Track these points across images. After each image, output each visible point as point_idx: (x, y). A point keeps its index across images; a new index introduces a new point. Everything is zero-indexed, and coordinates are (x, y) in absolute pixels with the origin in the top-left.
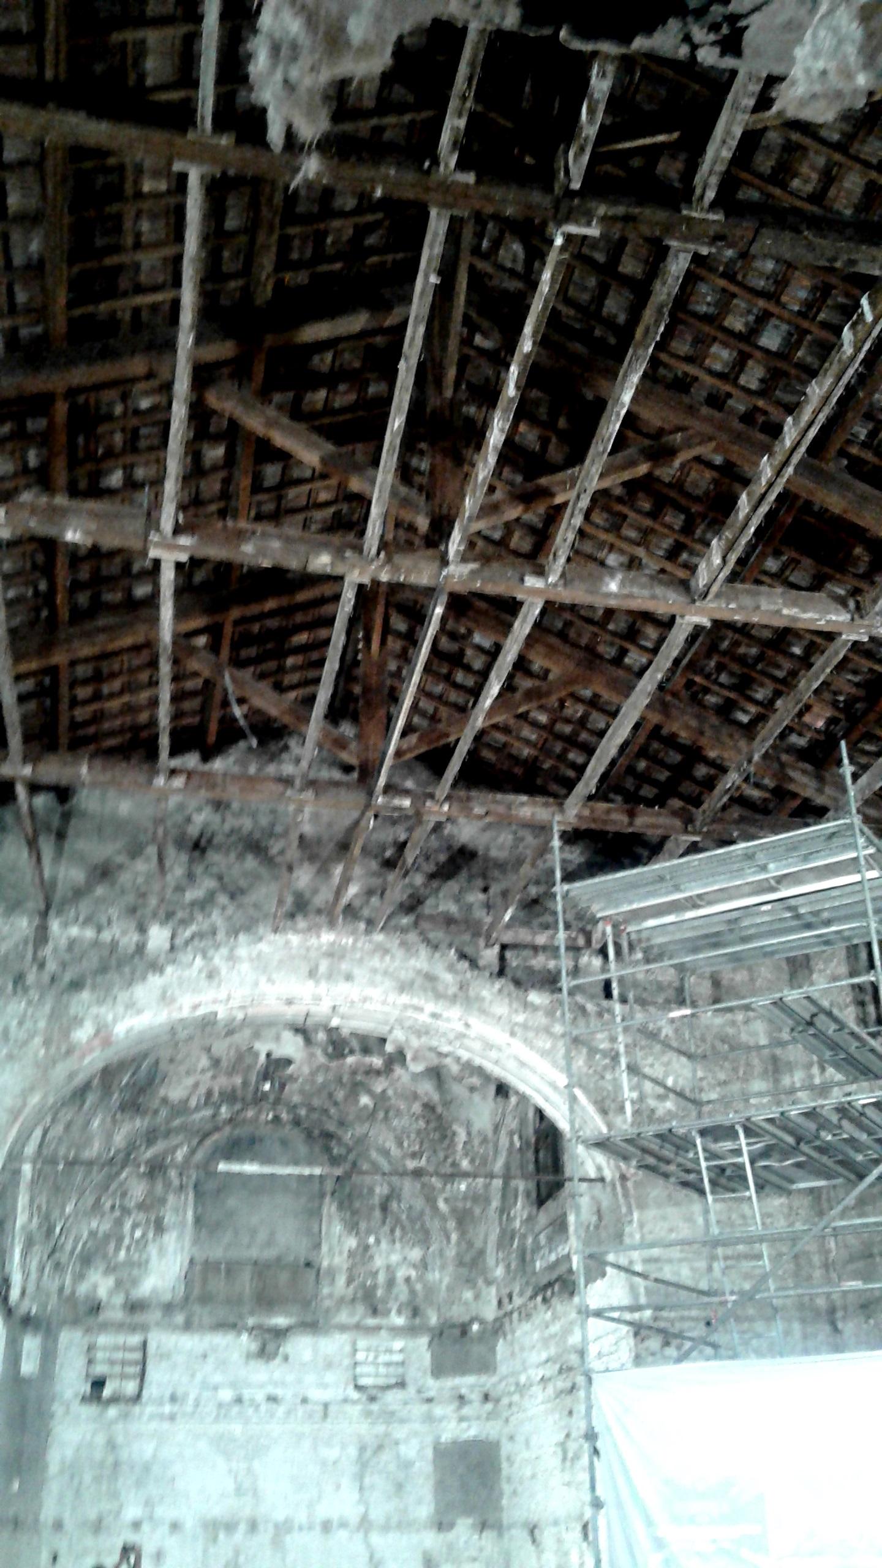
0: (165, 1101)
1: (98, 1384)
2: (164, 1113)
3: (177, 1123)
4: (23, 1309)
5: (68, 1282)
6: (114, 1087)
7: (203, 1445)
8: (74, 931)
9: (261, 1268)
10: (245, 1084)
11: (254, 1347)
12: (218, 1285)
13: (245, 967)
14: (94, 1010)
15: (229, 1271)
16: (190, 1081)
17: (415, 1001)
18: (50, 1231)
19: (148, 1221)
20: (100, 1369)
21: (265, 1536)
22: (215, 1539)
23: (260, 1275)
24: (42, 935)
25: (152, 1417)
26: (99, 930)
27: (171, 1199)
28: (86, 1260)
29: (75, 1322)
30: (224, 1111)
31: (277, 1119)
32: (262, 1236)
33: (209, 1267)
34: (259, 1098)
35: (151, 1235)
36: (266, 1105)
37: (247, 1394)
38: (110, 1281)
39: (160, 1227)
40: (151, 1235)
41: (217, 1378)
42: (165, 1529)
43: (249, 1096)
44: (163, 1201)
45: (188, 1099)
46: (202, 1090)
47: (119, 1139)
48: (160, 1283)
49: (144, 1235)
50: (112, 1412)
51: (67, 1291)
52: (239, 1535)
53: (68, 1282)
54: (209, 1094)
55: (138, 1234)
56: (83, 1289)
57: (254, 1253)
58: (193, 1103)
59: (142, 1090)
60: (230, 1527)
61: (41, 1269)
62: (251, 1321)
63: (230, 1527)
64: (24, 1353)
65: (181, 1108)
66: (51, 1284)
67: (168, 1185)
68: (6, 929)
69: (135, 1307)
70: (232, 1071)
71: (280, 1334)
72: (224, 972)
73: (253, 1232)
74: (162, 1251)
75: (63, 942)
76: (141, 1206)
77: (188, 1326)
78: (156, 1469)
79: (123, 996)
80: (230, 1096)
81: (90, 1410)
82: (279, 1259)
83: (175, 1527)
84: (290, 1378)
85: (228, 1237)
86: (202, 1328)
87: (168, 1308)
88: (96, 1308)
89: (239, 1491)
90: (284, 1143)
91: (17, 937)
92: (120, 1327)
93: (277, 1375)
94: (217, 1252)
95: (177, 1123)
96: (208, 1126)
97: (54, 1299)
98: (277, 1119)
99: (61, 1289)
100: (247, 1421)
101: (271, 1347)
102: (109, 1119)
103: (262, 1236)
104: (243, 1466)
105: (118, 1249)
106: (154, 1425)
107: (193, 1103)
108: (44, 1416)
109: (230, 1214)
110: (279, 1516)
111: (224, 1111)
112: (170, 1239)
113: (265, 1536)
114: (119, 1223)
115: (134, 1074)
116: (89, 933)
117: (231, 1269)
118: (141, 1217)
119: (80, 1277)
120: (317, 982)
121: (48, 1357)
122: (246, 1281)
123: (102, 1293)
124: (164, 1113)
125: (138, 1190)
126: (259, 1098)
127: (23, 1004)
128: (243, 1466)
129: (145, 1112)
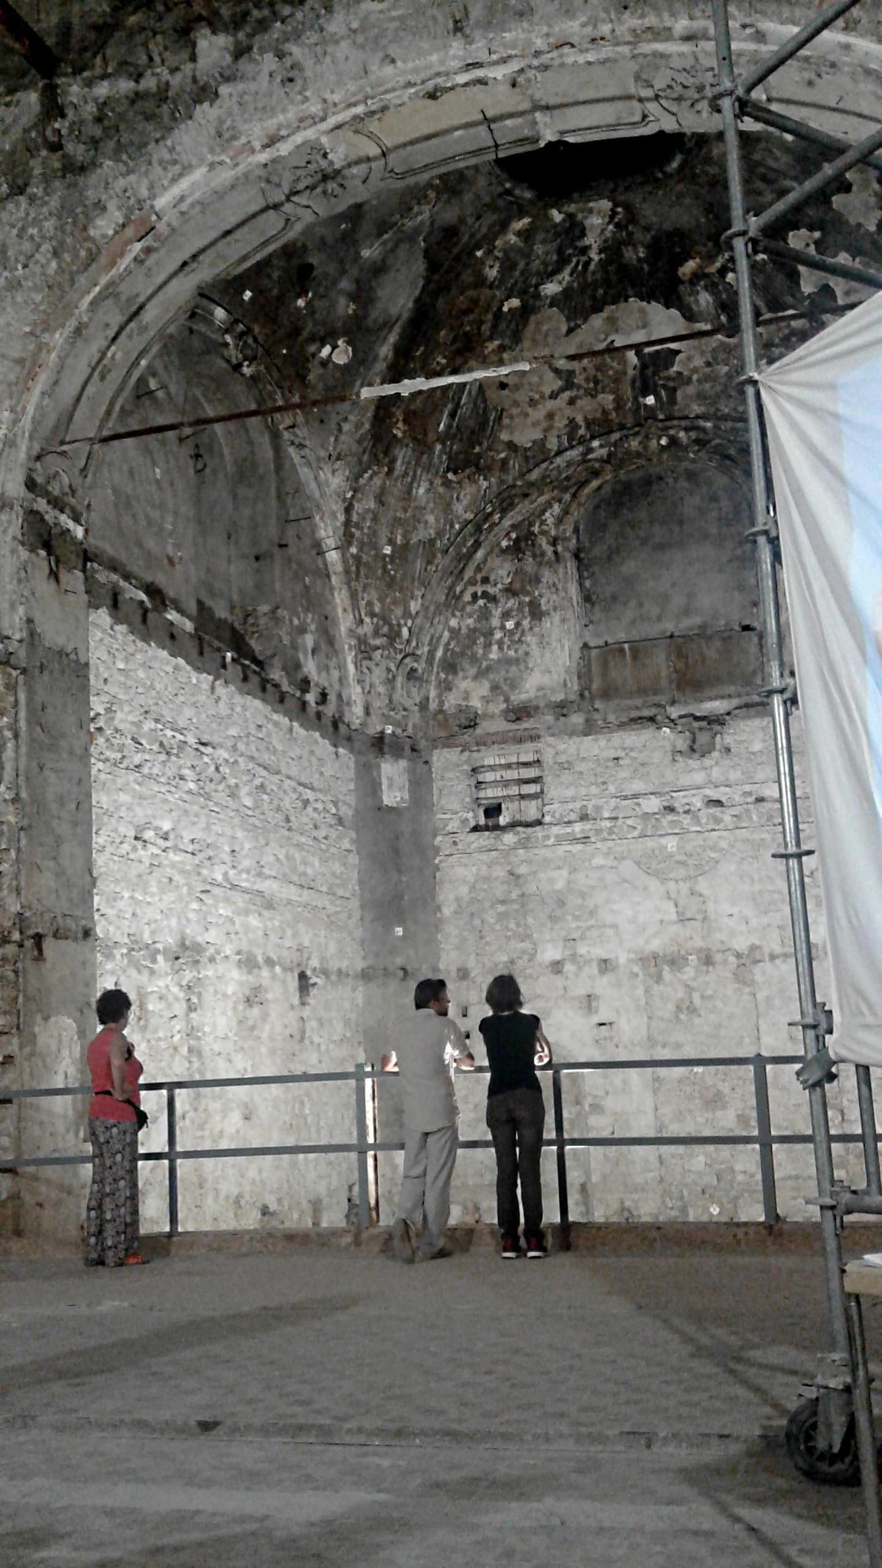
0: (511, 446)
1: (493, 811)
2: (515, 465)
3: (534, 475)
4: (375, 728)
5: (433, 694)
6: (432, 436)
7: (628, 868)
8: (102, 90)
9: (678, 644)
10: (619, 405)
11: (682, 743)
12: (623, 673)
13: (344, 49)
14: (121, 182)
15: (635, 656)
16: (538, 414)
17: (651, 20)
18: (393, 636)
19: (520, 609)
20: (491, 793)
21: (724, 970)
22: (659, 979)
23: (680, 654)
24: (53, 108)
25: (560, 840)
26: (138, 77)
27: (547, 576)
28: (451, 667)
29: (448, 742)
30: (599, 448)
31: (674, 441)
32: (678, 601)
33: (611, 652)
34: (643, 419)
35: (526, 623)
36: (653, 427)
37: (680, 800)
38: (483, 688)
39: (537, 613)
40: (526, 623)
41: (637, 786)
42: (594, 969)
43: (629, 421)
44: (537, 580)
45: (544, 440)
46: (560, 423)
47: (462, 510)
48: (546, 680)
49: (518, 624)
50: (509, 838)
51: (433, 706)
52: (689, 972)
53: (433, 694)
54: (572, 424)
55: (510, 625)
56: (452, 701)
57: (669, 626)
58: (553, 444)
59: (474, 437)
60: (676, 962)
61: (391, 681)
62: (674, 712)
63: (676, 962)
64: (384, 781)
65: (538, 454)
66: (407, 696)
67: (539, 556)
68: (9, 117)
69: (519, 713)
70: (595, 388)
71: (715, 721)
72: (308, 63)
73: (664, 599)
74: (543, 643)
75: (91, 109)
76: (510, 591)
77: (589, 729)
78: (573, 901)
79: (160, 152)
80: (601, 426)
81: (485, 839)
82: (703, 627)
83: (605, 965)
84: (734, 775)
85: (630, 614)
86: (608, 728)
87: (561, 709)
88: (472, 723)
89: (683, 919)
90: (691, 476)
91: (25, 121)
92: (502, 739)
93: (716, 773)
94: (619, 633)
95: (534, 475)
96: (581, 472)
97: (415, 718)
98: (674, 441)
99: (423, 706)
100: (682, 833)
101: (703, 738)
102: (438, 481)
103: (678, 601)
104: (685, 888)
105: (488, 646)
106: (561, 850)
107: (553, 444)
108: (426, 853)
109: (629, 581)
110: (741, 944)
111: (599, 448)
112: (551, 625)
113: (724, 970)
114: (485, 615)
115: (452, 415)
116: (125, 86)
117: (639, 650)
118: (511, 603)
119: (446, 687)
120: (468, 40)
121: (420, 784)
122: (661, 663)
123: (476, 703)
124: (515, 465)
125: (503, 572)
126: (643, 419)
127: (24, 205)
128: (685, 888)
129: (489, 468)
